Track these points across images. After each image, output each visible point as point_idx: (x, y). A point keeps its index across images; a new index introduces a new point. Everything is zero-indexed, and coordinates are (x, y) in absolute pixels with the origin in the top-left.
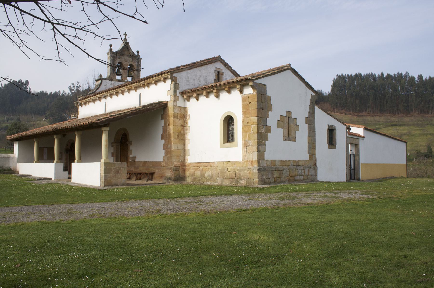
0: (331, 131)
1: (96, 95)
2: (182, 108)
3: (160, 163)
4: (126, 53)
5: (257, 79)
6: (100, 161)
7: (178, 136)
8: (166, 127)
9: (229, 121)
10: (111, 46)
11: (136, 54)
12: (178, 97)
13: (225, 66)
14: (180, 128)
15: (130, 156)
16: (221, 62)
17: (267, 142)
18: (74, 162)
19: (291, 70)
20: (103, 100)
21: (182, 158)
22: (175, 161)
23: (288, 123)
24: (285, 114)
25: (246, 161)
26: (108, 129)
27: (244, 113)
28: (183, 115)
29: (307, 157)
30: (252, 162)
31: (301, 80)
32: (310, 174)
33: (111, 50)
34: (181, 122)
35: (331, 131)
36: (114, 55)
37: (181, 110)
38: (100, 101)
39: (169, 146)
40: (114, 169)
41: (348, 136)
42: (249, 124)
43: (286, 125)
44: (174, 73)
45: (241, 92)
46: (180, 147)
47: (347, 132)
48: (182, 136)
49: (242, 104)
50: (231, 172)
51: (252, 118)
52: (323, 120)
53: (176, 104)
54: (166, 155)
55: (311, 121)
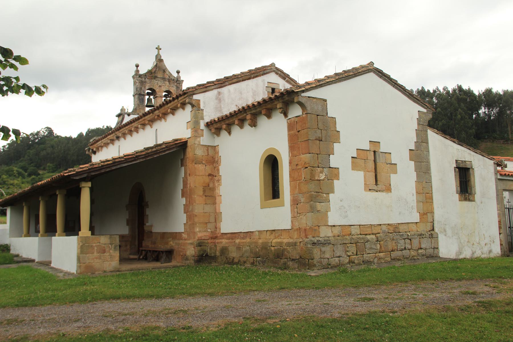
0: (464, 174)
1: (106, 136)
2: (210, 148)
3: (180, 233)
4: (160, 75)
5: (307, 90)
6: (78, 235)
7: (204, 191)
8: (187, 178)
9: (272, 163)
10: (137, 66)
11: (175, 75)
12: (202, 130)
13: (284, 79)
14: (207, 179)
15: (147, 224)
16: (277, 74)
17: (331, 195)
18: (55, 236)
19: (374, 72)
20: (117, 143)
21: (211, 226)
22: (200, 231)
23: (374, 164)
24: (367, 147)
25: (297, 229)
26: (89, 184)
27: (292, 148)
28: (213, 160)
29: (416, 217)
30: (305, 230)
31: (396, 88)
32: (423, 246)
33: (137, 71)
34: (208, 169)
35: (464, 174)
36: (140, 79)
37: (208, 150)
38: (113, 144)
39: (191, 207)
40: (96, 246)
41: (499, 177)
42: (299, 167)
43: (371, 165)
44: (194, 94)
45: (286, 115)
46: (208, 208)
47: (497, 172)
48: (210, 192)
49: (288, 135)
50: (276, 248)
51: (302, 156)
52: (446, 154)
53: (199, 142)
54: (187, 222)
55: (420, 156)
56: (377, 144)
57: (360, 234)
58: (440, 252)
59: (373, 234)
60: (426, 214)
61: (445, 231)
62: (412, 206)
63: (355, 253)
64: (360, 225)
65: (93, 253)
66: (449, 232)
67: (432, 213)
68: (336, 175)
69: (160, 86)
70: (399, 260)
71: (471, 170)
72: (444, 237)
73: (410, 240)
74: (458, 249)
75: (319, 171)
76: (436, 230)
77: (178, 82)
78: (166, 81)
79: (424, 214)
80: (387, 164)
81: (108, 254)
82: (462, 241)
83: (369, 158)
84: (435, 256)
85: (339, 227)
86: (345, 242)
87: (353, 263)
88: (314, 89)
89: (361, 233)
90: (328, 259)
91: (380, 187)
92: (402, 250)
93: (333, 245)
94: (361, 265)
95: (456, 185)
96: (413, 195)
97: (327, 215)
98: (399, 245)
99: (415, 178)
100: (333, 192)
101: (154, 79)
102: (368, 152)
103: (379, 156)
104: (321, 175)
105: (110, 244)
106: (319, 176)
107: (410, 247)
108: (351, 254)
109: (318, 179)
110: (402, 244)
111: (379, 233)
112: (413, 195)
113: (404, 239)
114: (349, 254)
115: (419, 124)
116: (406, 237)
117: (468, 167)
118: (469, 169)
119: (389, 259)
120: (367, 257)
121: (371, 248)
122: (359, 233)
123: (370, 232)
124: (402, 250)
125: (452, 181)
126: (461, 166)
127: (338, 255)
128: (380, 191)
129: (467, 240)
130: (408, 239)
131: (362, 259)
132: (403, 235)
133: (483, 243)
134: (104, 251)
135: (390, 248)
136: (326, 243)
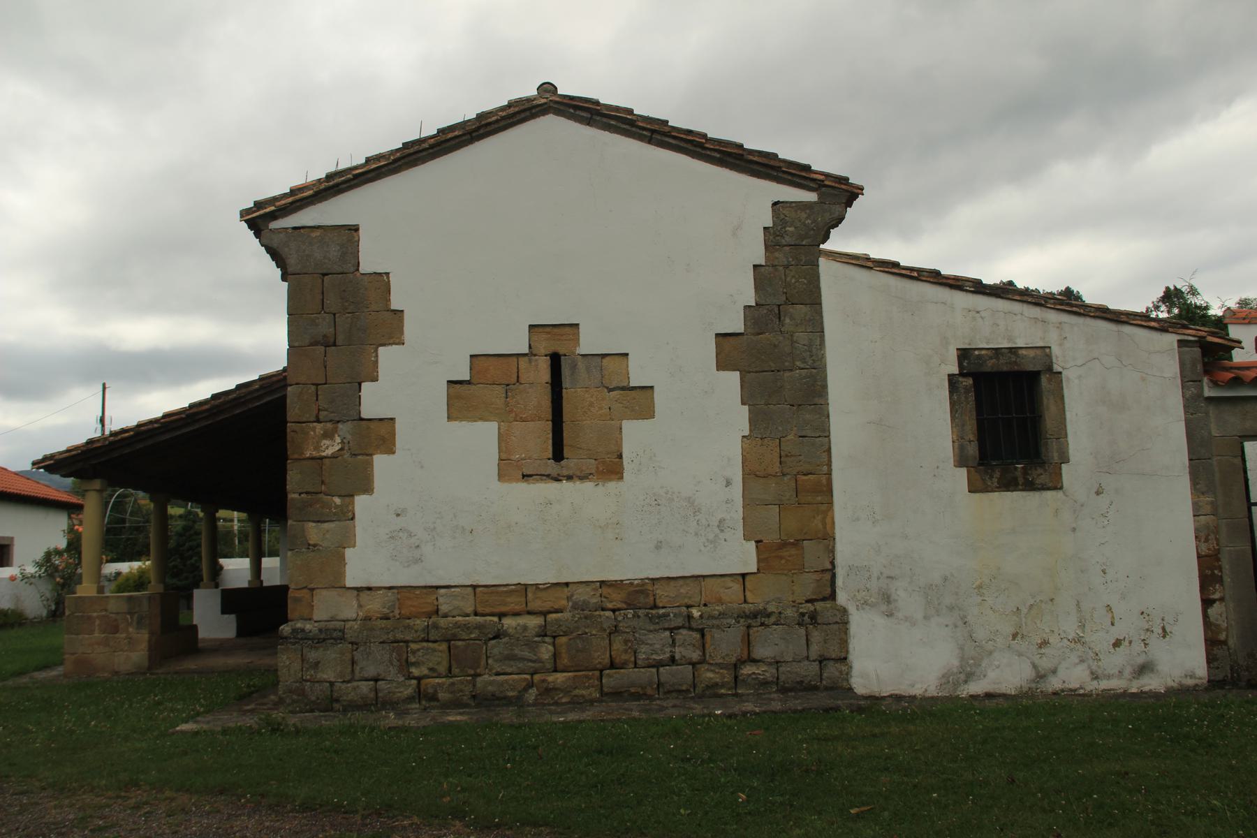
17: (361, 501)
32: (760, 651)
43: (539, 398)
56: (567, 329)
57: (476, 614)
59: (529, 613)
60: (797, 544)
61: (887, 598)
62: (721, 521)
63: (442, 669)
64: (474, 587)
65: (92, 632)
66: (909, 602)
67: (827, 538)
68: (384, 440)
70: (637, 697)
71: (1044, 380)
72: (880, 621)
73: (702, 632)
74: (956, 663)
76: (842, 598)
80: (610, 390)
81: (124, 635)
82: (980, 634)
84: (842, 688)
86: (400, 636)
87: (433, 698)
89: (480, 610)
90: (332, 684)
91: (570, 464)
93: (352, 643)
96: (728, 483)
97: (341, 559)
98: (644, 648)
100: (368, 489)
102: (523, 361)
104: (326, 442)
105: (129, 613)
106: (317, 448)
107: (695, 656)
109: (315, 454)
110: (655, 644)
112: (728, 483)
113: (671, 630)
114: (415, 671)
117: (1031, 368)
118: (1034, 377)
120: (491, 683)
121: (512, 658)
122: (470, 610)
124: (658, 665)
125: (934, 425)
127: (371, 671)
128: (569, 478)
129: (1009, 629)
130: (690, 629)
131: (468, 689)
132: (666, 615)
133: (1100, 639)
134: (116, 630)
136: (330, 636)
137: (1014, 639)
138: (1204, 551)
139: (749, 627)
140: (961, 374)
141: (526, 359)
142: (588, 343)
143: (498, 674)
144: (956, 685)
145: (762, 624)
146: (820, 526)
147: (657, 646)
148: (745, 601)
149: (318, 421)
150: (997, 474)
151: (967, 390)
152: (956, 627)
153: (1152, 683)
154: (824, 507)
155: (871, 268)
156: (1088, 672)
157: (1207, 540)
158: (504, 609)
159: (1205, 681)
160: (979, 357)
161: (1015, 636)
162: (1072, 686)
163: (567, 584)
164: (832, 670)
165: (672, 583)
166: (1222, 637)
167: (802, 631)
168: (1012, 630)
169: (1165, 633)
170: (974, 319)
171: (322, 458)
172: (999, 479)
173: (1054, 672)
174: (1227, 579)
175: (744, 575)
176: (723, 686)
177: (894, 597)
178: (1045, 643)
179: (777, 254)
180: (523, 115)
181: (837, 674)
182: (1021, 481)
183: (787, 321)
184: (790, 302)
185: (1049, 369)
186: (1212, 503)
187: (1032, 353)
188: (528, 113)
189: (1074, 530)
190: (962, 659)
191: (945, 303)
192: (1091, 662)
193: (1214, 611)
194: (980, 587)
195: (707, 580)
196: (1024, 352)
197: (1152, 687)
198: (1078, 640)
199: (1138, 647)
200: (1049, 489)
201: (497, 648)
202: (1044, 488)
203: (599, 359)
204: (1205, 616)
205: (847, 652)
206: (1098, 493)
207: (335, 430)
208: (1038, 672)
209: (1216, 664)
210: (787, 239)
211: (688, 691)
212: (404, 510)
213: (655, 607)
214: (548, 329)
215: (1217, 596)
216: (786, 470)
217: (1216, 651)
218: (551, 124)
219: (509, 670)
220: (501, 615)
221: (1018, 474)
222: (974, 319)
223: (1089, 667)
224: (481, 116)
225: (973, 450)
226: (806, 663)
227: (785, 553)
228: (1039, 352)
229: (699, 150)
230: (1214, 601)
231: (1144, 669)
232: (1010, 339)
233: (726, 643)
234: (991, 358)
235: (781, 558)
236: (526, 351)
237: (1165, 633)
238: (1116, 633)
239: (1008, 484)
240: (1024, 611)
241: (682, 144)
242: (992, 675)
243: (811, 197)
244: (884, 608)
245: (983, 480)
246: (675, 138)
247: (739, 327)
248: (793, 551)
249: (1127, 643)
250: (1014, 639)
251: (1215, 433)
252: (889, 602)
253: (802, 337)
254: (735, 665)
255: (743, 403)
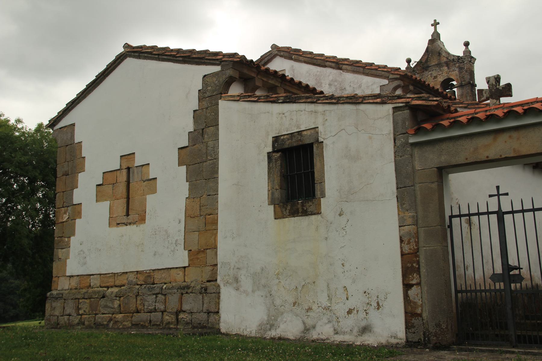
19: (130, 56)
32: (186, 307)
43: (121, 189)
56: (132, 156)
57: (101, 287)
58: (222, 320)
59: (116, 286)
61: (237, 280)
62: (176, 241)
64: (100, 274)
66: (246, 283)
69: (435, 77)
72: (233, 292)
74: (266, 318)
75: (63, 211)
77: (460, 61)
78: (442, 66)
79: (199, 252)
80: (144, 181)
82: (278, 302)
83: (120, 179)
84: (207, 328)
85: (78, 278)
88: (63, 117)
90: (58, 316)
92: (150, 312)
93: (65, 299)
94: (92, 328)
95: (322, 182)
96: (180, 222)
98: (146, 303)
99: (185, 192)
101: (426, 70)
103: (133, 173)
104: (65, 215)
107: (162, 308)
108: (83, 312)
111: (124, 286)
112: (180, 222)
114: (81, 312)
115: (200, 100)
116: (157, 291)
117: (308, 141)
118: (311, 146)
119: (128, 324)
121: (106, 306)
122: (98, 285)
123: (112, 284)
126: (286, 146)
129: (291, 300)
130: (162, 294)
133: (340, 309)
135: (133, 307)
137: (294, 306)
138: (407, 249)
139: (182, 294)
140: (274, 151)
141: (119, 171)
142: (138, 161)
143: (103, 314)
144: (265, 331)
145: (187, 293)
146: (213, 241)
147: (150, 302)
148: (185, 281)
149: (63, 207)
150: (289, 208)
151: (276, 160)
152: (266, 297)
153: (370, 340)
154: (215, 232)
155: (238, 100)
156: (332, 329)
157: (409, 243)
158: (108, 284)
159: (404, 341)
160: (283, 140)
161: (294, 304)
162: (323, 337)
163: (127, 273)
164: (212, 318)
165: (160, 272)
166: (419, 311)
167: (201, 297)
168: (294, 301)
169: (378, 307)
170: (282, 118)
171: (63, 222)
172: (290, 210)
173: (314, 327)
174: (423, 270)
175: (185, 267)
176: (172, 323)
177: (239, 279)
178: (309, 309)
179: (203, 103)
180: (118, 61)
181: (214, 320)
182: (300, 210)
183: (206, 136)
184: (207, 126)
185: (317, 140)
186: (413, 217)
187: (309, 133)
188: (119, 60)
189: (326, 239)
190: (269, 316)
191: (268, 112)
192: (334, 323)
193: (412, 292)
194: (278, 274)
195: (172, 270)
196: (305, 133)
197: (368, 342)
198: (327, 308)
199: (362, 315)
200: (314, 214)
201: (102, 302)
202: (313, 214)
203: (141, 167)
204: (406, 296)
205: (219, 309)
206: (340, 215)
207: (67, 210)
208: (305, 327)
209: (413, 330)
210: (208, 94)
211: (159, 325)
212: (82, 242)
213: (153, 284)
214: (126, 157)
215: (414, 282)
216: (202, 213)
217: (413, 321)
218: (129, 62)
219: (105, 312)
220: (108, 287)
221: (299, 206)
222: (282, 118)
223: (333, 326)
224: (262, 57)
225: (277, 194)
226: (202, 314)
227: (199, 256)
228: (312, 131)
229: (175, 58)
230: (412, 285)
231: (365, 330)
232: (298, 127)
233: (173, 302)
234: (288, 140)
235: (198, 259)
236: (119, 168)
237: (378, 307)
238: (350, 304)
239: (294, 213)
240: (300, 288)
241: (169, 58)
242: (282, 326)
243: (217, 68)
244: (235, 285)
245: (282, 212)
246: (166, 55)
247: (186, 144)
248: (203, 255)
249: (355, 312)
250: (294, 306)
251: (418, 167)
252: (237, 282)
253: (211, 144)
254: (176, 313)
255: (187, 181)
